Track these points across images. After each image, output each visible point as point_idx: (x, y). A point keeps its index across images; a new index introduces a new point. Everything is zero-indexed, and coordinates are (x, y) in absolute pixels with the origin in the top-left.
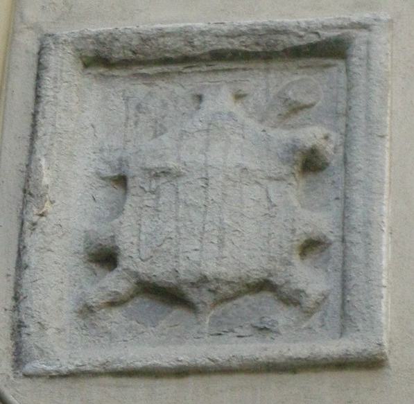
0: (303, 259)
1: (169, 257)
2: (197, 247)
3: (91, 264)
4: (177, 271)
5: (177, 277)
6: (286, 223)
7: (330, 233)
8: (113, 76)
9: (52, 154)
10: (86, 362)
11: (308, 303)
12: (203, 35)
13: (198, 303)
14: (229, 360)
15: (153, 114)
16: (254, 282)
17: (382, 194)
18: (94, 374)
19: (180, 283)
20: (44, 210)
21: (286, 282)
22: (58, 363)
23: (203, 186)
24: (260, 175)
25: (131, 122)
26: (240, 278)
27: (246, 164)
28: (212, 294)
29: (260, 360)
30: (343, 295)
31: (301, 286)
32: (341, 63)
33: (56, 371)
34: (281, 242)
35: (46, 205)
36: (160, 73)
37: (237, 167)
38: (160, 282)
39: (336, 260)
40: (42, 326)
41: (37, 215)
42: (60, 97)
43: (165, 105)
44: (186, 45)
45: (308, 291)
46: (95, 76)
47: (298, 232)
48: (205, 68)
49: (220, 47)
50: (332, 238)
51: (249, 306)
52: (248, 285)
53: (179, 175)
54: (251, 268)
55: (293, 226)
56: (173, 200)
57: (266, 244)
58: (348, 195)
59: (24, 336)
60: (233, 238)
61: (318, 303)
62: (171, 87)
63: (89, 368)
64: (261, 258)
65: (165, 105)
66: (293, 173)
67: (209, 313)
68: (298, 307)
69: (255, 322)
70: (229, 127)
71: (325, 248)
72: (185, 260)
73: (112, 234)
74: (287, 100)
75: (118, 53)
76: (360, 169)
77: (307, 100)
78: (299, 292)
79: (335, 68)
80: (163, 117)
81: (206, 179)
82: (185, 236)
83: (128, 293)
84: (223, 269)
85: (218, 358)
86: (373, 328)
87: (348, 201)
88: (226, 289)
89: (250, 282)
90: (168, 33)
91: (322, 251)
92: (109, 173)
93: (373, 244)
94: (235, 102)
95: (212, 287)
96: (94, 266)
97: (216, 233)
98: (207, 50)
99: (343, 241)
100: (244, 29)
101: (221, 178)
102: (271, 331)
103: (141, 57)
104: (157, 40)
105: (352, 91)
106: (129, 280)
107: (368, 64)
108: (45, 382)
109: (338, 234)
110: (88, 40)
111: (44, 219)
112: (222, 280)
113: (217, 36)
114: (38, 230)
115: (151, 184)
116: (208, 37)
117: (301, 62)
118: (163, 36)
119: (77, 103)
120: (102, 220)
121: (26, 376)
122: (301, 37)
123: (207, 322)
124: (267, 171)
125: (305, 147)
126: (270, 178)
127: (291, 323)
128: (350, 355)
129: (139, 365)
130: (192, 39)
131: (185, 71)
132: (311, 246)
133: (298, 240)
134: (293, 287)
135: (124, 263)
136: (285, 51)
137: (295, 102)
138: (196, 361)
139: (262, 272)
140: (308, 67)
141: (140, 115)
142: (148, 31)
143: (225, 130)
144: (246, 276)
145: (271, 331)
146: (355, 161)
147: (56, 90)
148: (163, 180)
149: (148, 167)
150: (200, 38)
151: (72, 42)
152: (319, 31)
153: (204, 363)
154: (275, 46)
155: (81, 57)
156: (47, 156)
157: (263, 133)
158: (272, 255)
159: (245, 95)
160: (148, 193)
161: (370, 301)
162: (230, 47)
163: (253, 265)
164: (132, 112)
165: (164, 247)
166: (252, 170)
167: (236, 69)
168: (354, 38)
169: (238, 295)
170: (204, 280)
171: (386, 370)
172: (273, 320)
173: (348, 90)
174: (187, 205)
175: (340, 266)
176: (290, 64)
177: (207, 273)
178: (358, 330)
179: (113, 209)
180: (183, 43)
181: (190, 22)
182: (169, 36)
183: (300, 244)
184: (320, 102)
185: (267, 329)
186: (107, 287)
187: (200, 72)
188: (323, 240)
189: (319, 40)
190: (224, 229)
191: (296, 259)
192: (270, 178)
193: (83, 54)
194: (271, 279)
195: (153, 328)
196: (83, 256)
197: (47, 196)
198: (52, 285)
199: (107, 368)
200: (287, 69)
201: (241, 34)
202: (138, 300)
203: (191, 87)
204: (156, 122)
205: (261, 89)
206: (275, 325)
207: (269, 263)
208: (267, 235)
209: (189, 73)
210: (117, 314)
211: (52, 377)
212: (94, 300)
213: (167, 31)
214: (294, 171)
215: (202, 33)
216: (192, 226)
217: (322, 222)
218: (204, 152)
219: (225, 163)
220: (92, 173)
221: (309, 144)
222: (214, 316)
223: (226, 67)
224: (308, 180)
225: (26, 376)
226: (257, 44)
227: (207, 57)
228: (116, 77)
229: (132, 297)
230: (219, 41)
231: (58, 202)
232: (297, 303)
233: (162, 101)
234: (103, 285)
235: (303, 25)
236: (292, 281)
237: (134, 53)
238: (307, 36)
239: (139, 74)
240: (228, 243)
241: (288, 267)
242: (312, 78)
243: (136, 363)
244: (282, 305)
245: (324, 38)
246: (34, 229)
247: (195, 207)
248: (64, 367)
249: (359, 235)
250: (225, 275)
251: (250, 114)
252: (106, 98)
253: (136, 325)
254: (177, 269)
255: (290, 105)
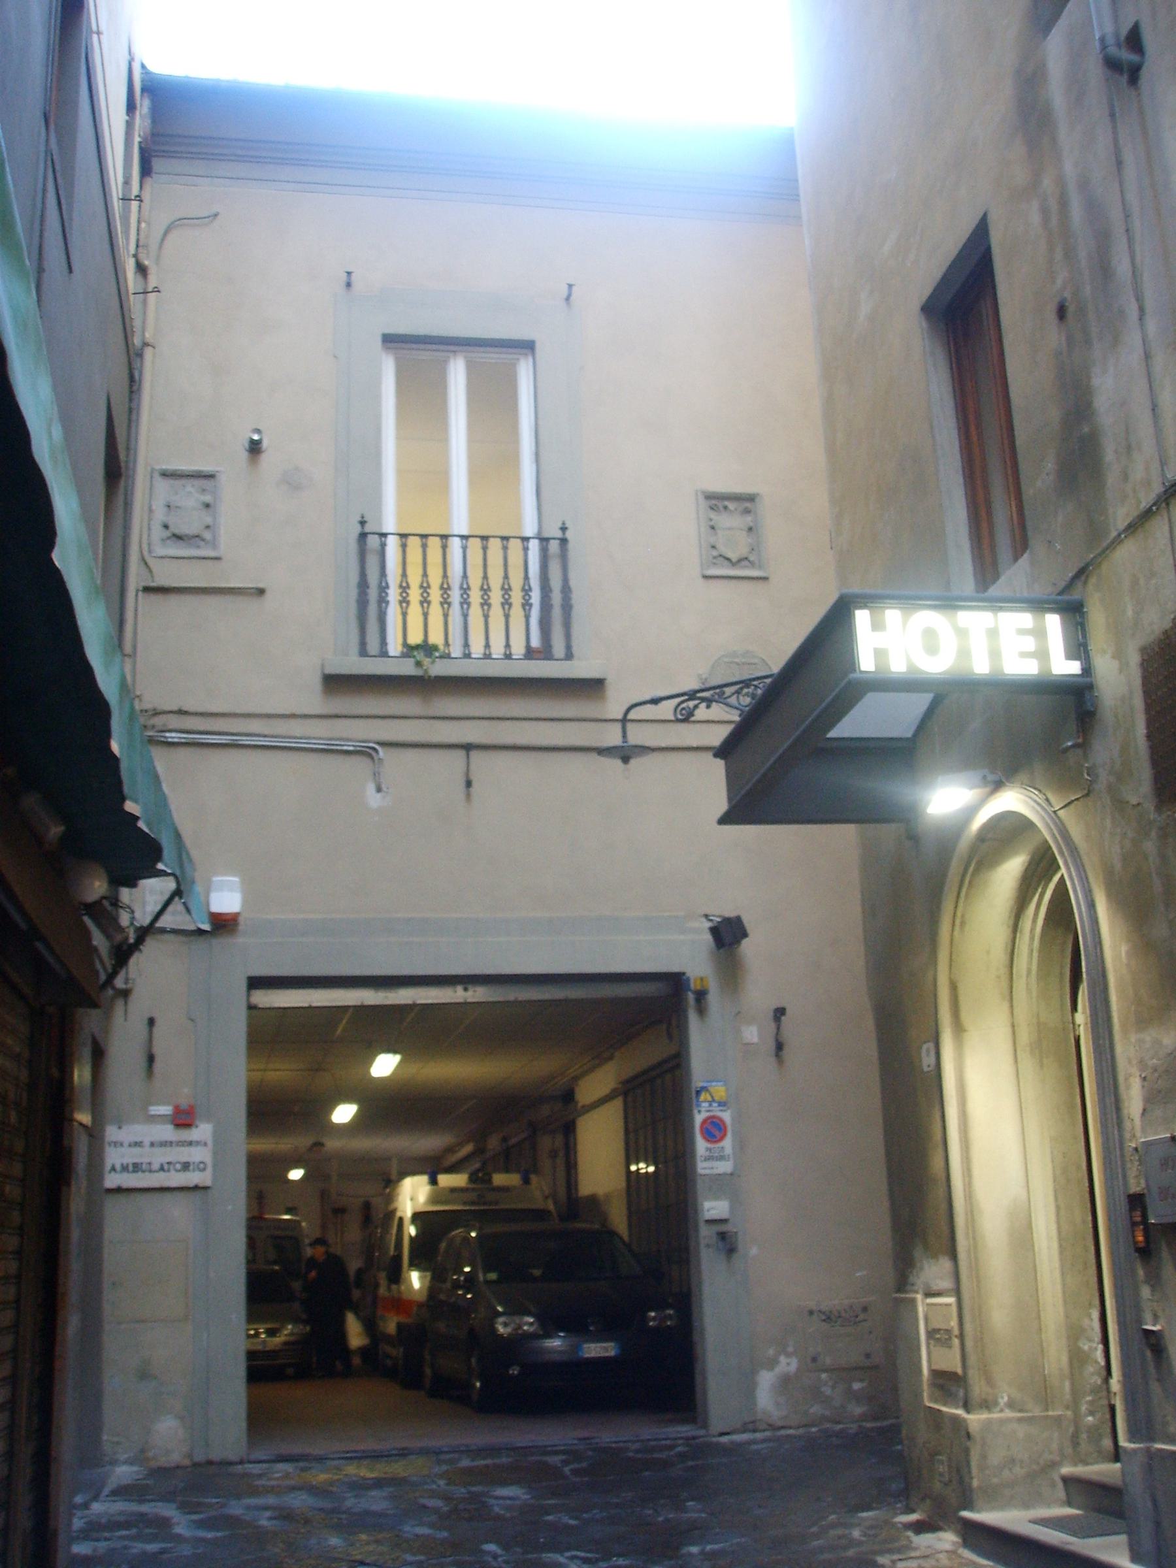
70: (301, 1536)
121: (152, 557)
132: (208, 527)
163: (195, 532)
210: (168, 541)
217: (209, 520)
225: (152, 557)
227: (384, 650)
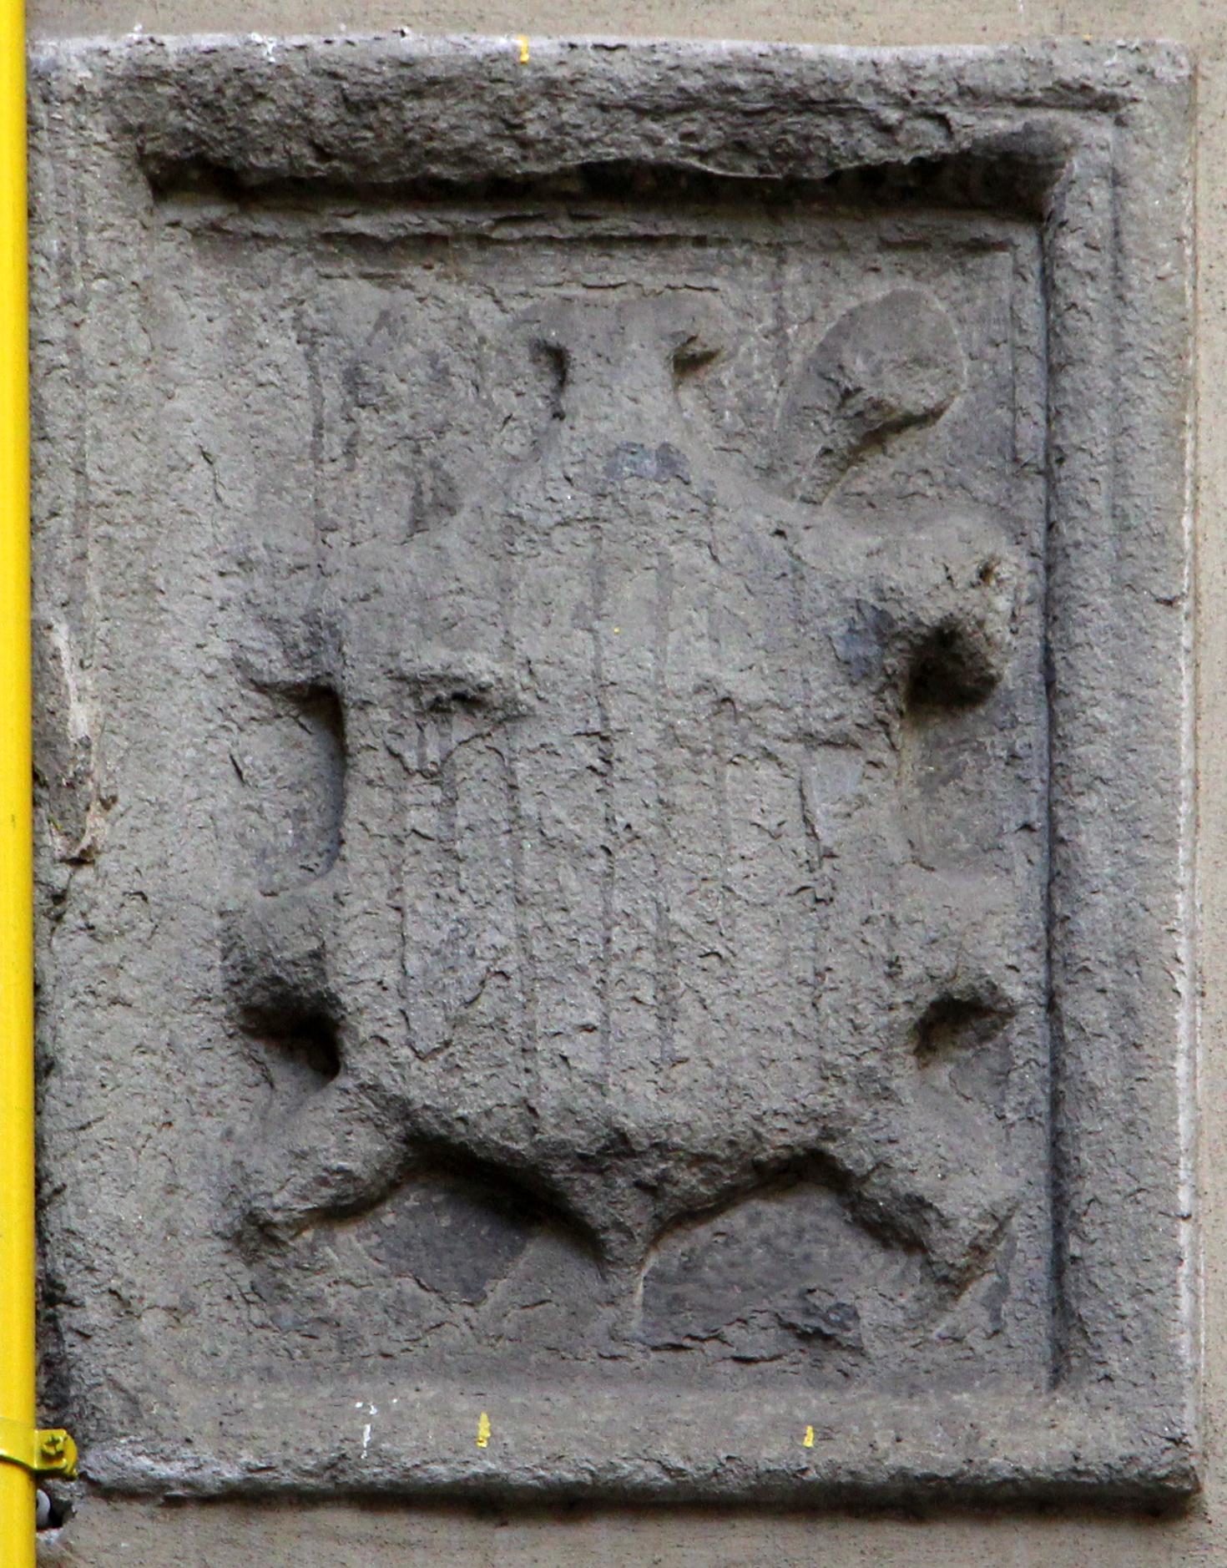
0: (926, 1065)
1: (504, 1051)
2: (592, 1017)
3: (255, 1044)
4: (532, 1110)
5: (535, 1130)
6: (867, 932)
7: (1009, 973)
8: (256, 236)
9: (87, 598)
10: (277, 1456)
11: (950, 1251)
12: (553, 98)
13: (605, 1229)
14: (715, 1474)
15: (404, 415)
16: (777, 1158)
17: (1171, 844)
18: (301, 1499)
19: (545, 1156)
20: (86, 841)
21: (877, 1166)
22: (187, 1452)
23: (592, 768)
24: (777, 724)
25: (334, 445)
26: (731, 1143)
27: (729, 680)
28: (648, 1198)
29: (812, 1475)
30: (1058, 1228)
31: (923, 1184)
32: (1025, 240)
33: (186, 1484)
34: (855, 1008)
35: (89, 824)
36: (414, 237)
37: (698, 690)
38: (481, 1144)
39: (1030, 1081)
40: (125, 1306)
41: (63, 860)
42: (90, 341)
43: (441, 376)
44: (496, 136)
45: (947, 1207)
46: (196, 233)
47: (910, 971)
48: (566, 228)
49: (614, 153)
50: (1015, 991)
51: (765, 1241)
52: (758, 1167)
53: (511, 716)
54: (764, 1105)
55: (891, 949)
56: (501, 815)
57: (808, 1010)
58: (1062, 832)
59: (69, 1338)
60: (700, 980)
61: (978, 1250)
62: (453, 293)
63: (287, 1478)
64: (795, 1065)
65: (441, 376)
66: (882, 723)
67: (640, 1264)
68: (918, 1258)
69: (785, 1303)
71: (996, 1027)
72: (554, 1066)
73: (314, 945)
74: (847, 394)
75: (268, 151)
76: (1100, 729)
77: (913, 395)
78: (918, 1204)
79: (1001, 255)
80: (440, 433)
81: (604, 739)
82: (548, 969)
83: (381, 1173)
84: (679, 1110)
85: (681, 1465)
86: (1153, 1376)
87: (1062, 851)
88: (689, 1179)
89: (762, 1157)
90: (433, 81)
91: (985, 1038)
92: (281, 672)
93: (1147, 1049)
94: (677, 385)
95: (648, 1173)
96: (260, 1049)
97: (646, 959)
98: (575, 157)
99: (1051, 1006)
100: (694, 83)
101: (650, 739)
102: (838, 1345)
103: (347, 169)
104: (400, 108)
105: (1065, 382)
106: (380, 1127)
107: (1118, 275)
108: (152, 1518)
109: (1031, 976)
110: (160, 89)
111: (85, 875)
112: (677, 1148)
113: (603, 108)
114: (72, 919)
115: (422, 743)
116: (572, 107)
117: (888, 226)
118: (417, 94)
119: (148, 361)
120: (271, 861)
122: (886, 129)
123: (638, 1299)
124: (798, 710)
125: (919, 623)
126: (809, 739)
127: (899, 1318)
128: (1088, 1473)
129: (442, 1472)
130: (517, 113)
131: (499, 233)
133: (909, 1004)
134: (906, 1185)
135: (362, 1062)
136: (836, 178)
137: (877, 405)
138: (613, 1467)
139: (799, 1123)
140: (909, 246)
141: (364, 414)
142: (365, 70)
143: (652, 523)
144: (749, 1133)
145: (838, 1345)
146: (1085, 694)
147: (74, 313)
148: (462, 727)
149: (407, 669)
150: (544, 107)
151: (107, 97)
152: (944, 109)
153: (640, 1478)
154: (802, 158)
155: (142, 158)
156: (72, 607)
157: (777, 542)
158: (828, 1057)
159: (708, 357)
160: (418, 779)
161: (1144, 1273)
162: (648, 152)
164: (333, 395)
165: (484, 1004)
166: (749, 706)
167: (673, 241)
168: (1066, 149)
169: (728, 1199)
170: (620, 1145)
171: (1198, 1527)
172: (840, 1306)
173: (1053, 371)
174: (549, 844)
175: (1044, 1107)
176: (849, 231)
177: (630, 1125)
178: (1107, 1378)
179: (300, 815)
180: (487, 127)
181: (506, 30)
182: (440, 96)
183: (916, 1016)
184: (958, 401)
185: (827, 1338)
186: (313, 1150)
187: (550, 241)
188: (987, 1002)
189: (948, 150)
190: (673, 946)
191: (904, 1075)
192: (809, 739)
193: (149, 147)
194: (831, 1147)
195: (468, 1311)
196: (223, 1009)
197: (90, 785)
198: (139, 1142)
199: (342, 1479)
200: (845, 248)
201: (690, 103)
202: (412, 1199)
203: (526, 304)
204: (417, 451)
205: (757, 328)
206: (850, 1323)
207: (822, 1090)
208: (811, 978)
209: (512, 242)
211: (174, 1503)
212: (277, 1200)
213: (430, 72)
214: (882, 714)
215: (551, 89)
216: (570, 932)
218: (588, 616)
219: (660, 674)
220: (222, 661)
221: (932, 613)
222: (658, 1276)
223: (638, 229)
224: (930, 734)
226: (742, 148)
228: (274, 240)
229: (394, 1187)
230: (612, 127)
231: (124, 798)
232: (914, 1245)
233: (433, 358)
234: (303, 1144)
235: (895, 82)
236: (896, 1164)
237: (322, 153)
238: (908, 125)
239: (343, 234)
240: (687, 1002)
241: (881, 1106)
242: (926, 290)
243: (432, 1467)
244: (867, 1243)
245: (966, 145)
246: (58, 918)
247: (577, 853)
248: (207, 1471)
249: (1101, 999)
250: (686, 1133)
251: (729, 436)
252: (239, 332)
253: (414, 1298)
254: (533, 1103)
255: (859, 414)
